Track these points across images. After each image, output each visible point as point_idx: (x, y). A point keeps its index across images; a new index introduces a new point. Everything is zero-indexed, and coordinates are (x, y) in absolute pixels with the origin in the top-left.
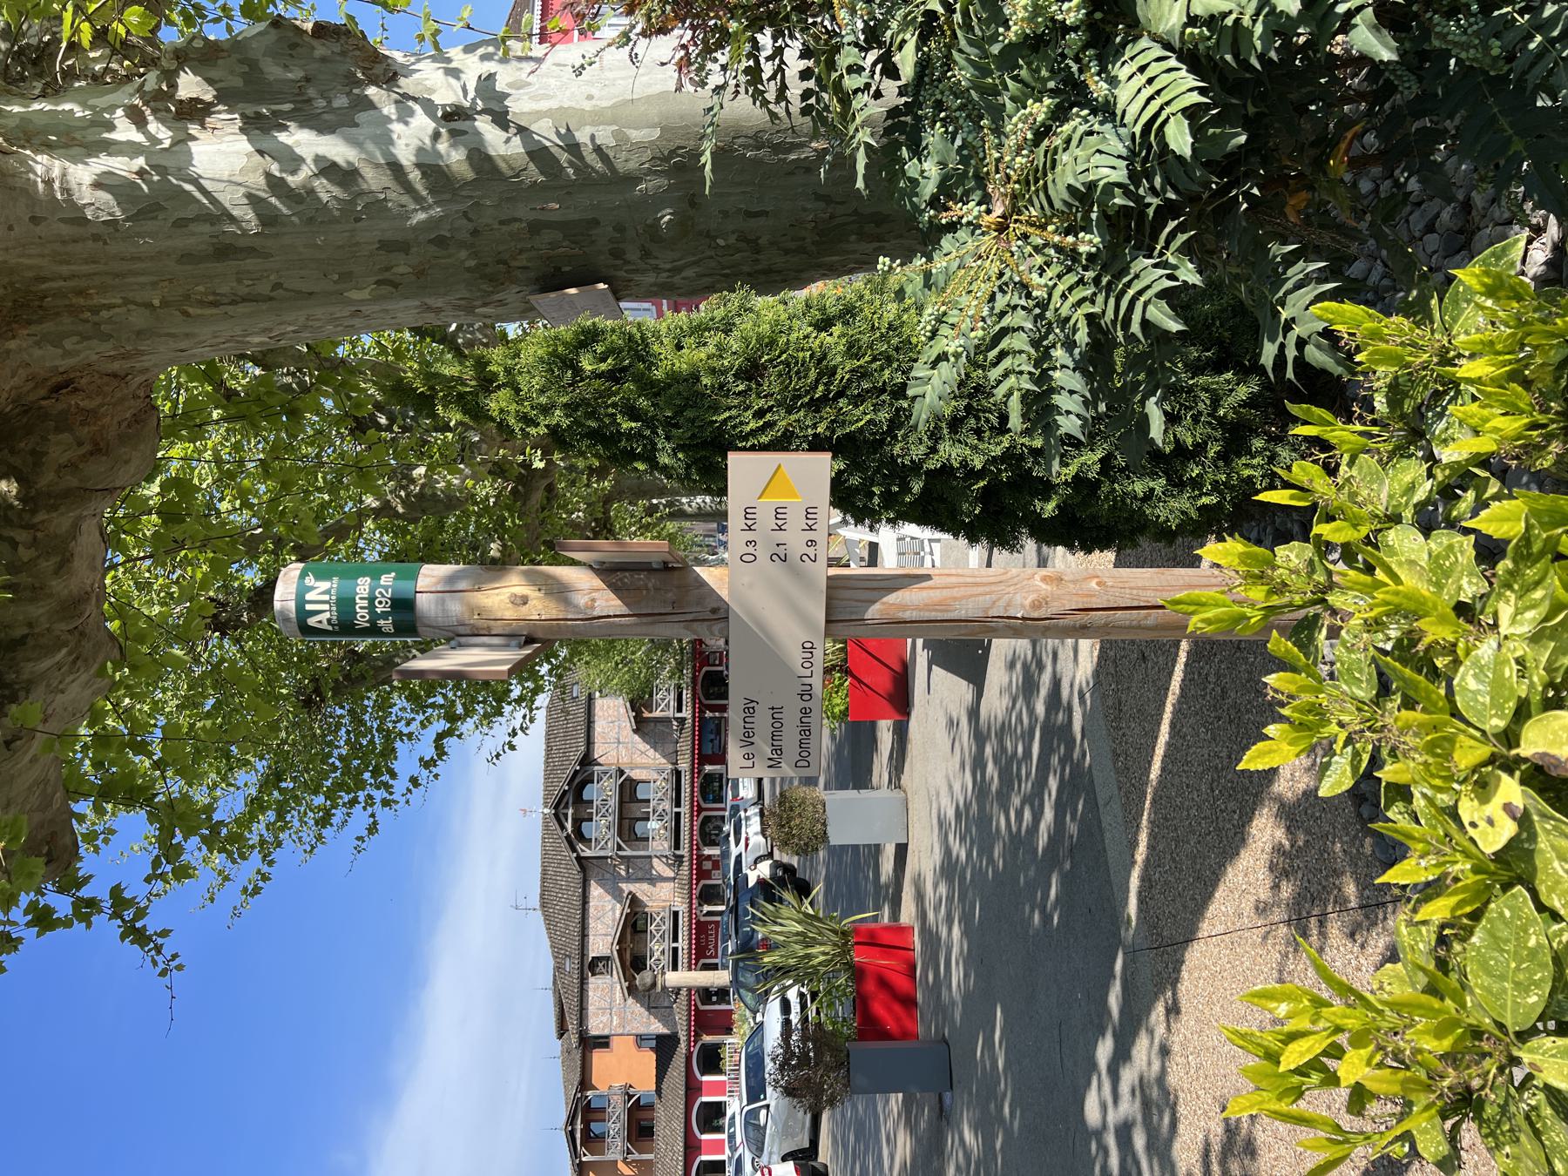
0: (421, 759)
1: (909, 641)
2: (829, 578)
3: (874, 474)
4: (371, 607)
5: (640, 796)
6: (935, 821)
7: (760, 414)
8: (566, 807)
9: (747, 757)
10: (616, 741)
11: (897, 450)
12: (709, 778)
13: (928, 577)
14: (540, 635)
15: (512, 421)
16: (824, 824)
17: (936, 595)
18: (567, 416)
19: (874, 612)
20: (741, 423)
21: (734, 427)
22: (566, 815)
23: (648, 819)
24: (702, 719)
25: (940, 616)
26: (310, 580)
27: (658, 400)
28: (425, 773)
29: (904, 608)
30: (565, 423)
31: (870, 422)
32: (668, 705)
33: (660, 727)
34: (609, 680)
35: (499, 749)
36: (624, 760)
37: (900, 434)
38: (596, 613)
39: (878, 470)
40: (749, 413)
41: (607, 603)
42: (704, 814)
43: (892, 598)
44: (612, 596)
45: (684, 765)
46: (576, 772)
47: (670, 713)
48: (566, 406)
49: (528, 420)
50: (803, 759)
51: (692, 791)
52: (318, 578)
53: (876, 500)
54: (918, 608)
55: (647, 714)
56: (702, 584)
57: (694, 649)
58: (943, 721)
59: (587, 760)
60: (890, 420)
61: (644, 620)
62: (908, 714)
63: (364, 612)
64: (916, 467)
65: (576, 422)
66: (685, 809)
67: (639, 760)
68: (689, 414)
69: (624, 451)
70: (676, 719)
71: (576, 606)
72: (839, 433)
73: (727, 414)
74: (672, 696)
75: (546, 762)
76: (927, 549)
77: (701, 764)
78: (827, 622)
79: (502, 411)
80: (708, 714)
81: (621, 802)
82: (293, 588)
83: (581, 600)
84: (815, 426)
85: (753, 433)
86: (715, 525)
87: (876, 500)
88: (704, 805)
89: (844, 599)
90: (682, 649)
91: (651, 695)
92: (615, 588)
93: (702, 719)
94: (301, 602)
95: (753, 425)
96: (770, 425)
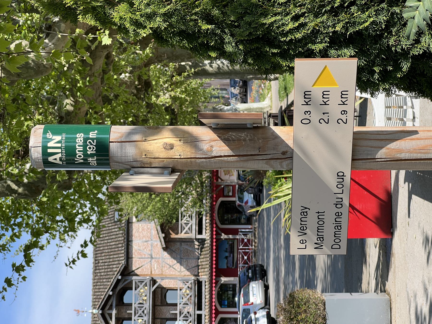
0: (14, 265)
1: (393, 173)
2: (354, 133)
3: (375, 58)
4: (85, 151)
5: (169, 301)
6: (413, 317)
7: (296, 18)
8: (111, 308)
9: (302, 242)
10: (149, 255)
11: (392, 42)
12: (224, 288)
13: (416, 132)
14: (179, 168)
15: (128, 25)
16: (324, 318)
17: (421, 143)
18: (165, 21)
19: (382, 154)
20: (283, 25)
21: (278, 27)
22: (110, 315)
23: (176, 319)
24: (218, 240)
25: (419, 156)
26: (49, 135)
27: (226, 10)
28: (16, 275)
29: (400, 151)
30: (164, 25)
31: (373, 23)
32: (190, 229)
33: (184, 246)
34: (145, 207)
35: (75, 256)
36: (156, 272)
37: (394, 30)
38: (214, 154)
39: (378, 56)
40: (289, 17)
41: (220, 148)
42: (220, 316)
43: (393, 145)
44: (223, 144)
45: (204, 277)
46: (118, 281)
47: (193, 235)
48: (164, 15)
49: (138, 25)
50: (337, 244)
51: (211, 298)
52: (54, 134)
53: (376, 76)
54: (409, 152)
55: (173, 236)
56: (276, 137)
57: (212, 183)
58: (420, 239)
59: (127, 272)
60: (387, 21)
61: (242, 158)
62: (392, 234)
63: (80, 154)
64: (405, 54)
65: (171, 25)
66: (205, 312)
67: (167, 272)
68: (247, 19)
69: (202, 45)
70: (198, 240)
71: (201, 150)
72: (351, 30)
73: (273, 19)
74: (194, 222)
75: (95, 273)
76: (409, 104)
77: (218, 276)
78: (353, 160)
79: (121, 18)
80: (224, 236)
81: (154, 306)
82: (40, 140)
83: (205, 147)
84: (334, 26)
85: (291, 31)
86: (228, 81)
87: (376, 76)
88: (220, 309)
89: (365, 145)
90: (202, 183)
91: (177, 221)
92: (226, 141)
93: (218, 240)
94: (45, 148)
95: (291, 26)
96: (303, 25)
